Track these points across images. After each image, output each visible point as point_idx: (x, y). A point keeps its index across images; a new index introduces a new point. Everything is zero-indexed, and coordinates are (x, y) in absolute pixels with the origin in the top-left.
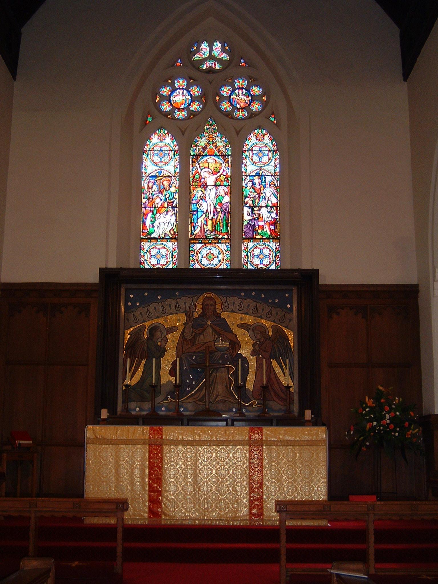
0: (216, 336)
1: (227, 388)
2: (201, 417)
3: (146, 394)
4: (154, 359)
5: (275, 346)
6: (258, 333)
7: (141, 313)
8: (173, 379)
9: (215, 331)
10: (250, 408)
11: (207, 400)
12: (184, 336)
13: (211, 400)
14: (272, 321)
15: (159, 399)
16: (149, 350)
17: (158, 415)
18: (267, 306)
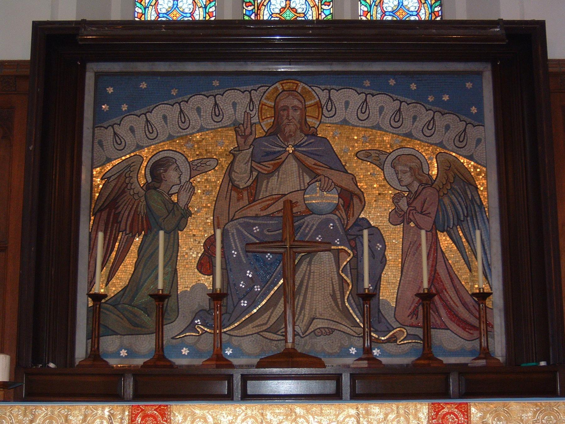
0: (307, 179)
1: (335, 300)
2: (275, 370)
3: (145, 317)
4: (161, 233)
5: (446, 200)
6: (405, 172)
7: (132, 130)
8: (206, 281)
9: (304, 167)
10: (390, 347)
11: (290, 329)
12: (231, 180)
13: (297, 328)
14: (436, 144)
15: (171, 330)
16: (143, 211)
17: (171, 365)
18: (423, 110)
